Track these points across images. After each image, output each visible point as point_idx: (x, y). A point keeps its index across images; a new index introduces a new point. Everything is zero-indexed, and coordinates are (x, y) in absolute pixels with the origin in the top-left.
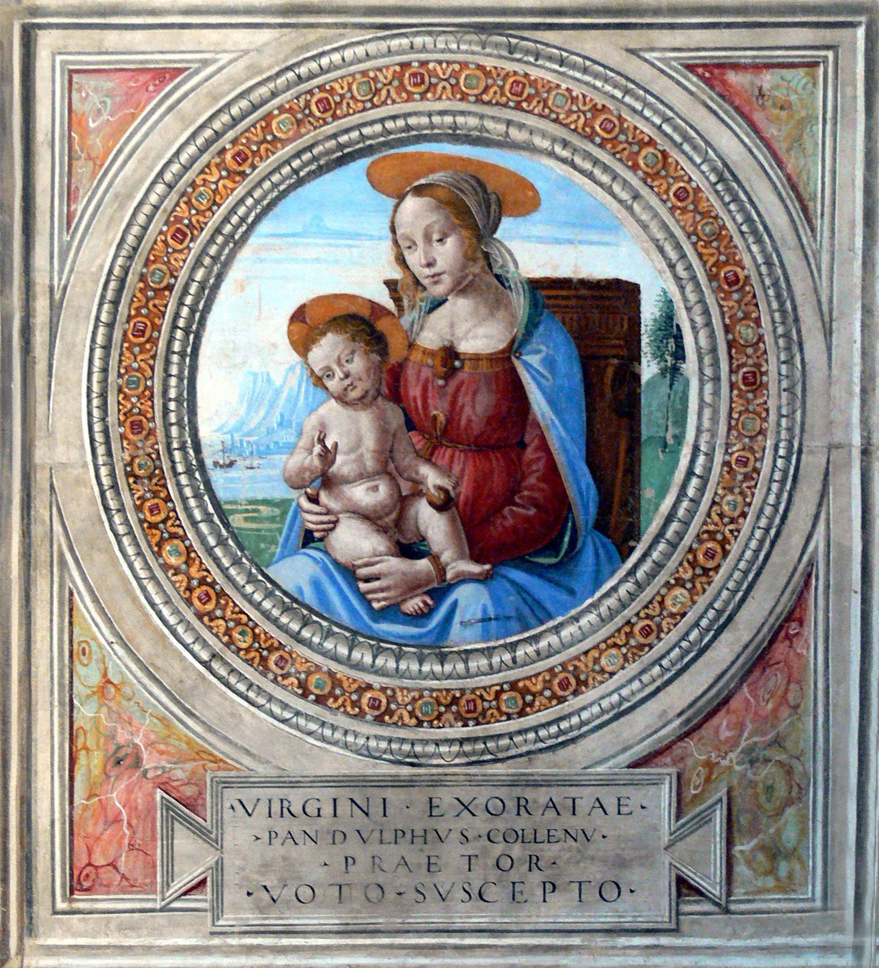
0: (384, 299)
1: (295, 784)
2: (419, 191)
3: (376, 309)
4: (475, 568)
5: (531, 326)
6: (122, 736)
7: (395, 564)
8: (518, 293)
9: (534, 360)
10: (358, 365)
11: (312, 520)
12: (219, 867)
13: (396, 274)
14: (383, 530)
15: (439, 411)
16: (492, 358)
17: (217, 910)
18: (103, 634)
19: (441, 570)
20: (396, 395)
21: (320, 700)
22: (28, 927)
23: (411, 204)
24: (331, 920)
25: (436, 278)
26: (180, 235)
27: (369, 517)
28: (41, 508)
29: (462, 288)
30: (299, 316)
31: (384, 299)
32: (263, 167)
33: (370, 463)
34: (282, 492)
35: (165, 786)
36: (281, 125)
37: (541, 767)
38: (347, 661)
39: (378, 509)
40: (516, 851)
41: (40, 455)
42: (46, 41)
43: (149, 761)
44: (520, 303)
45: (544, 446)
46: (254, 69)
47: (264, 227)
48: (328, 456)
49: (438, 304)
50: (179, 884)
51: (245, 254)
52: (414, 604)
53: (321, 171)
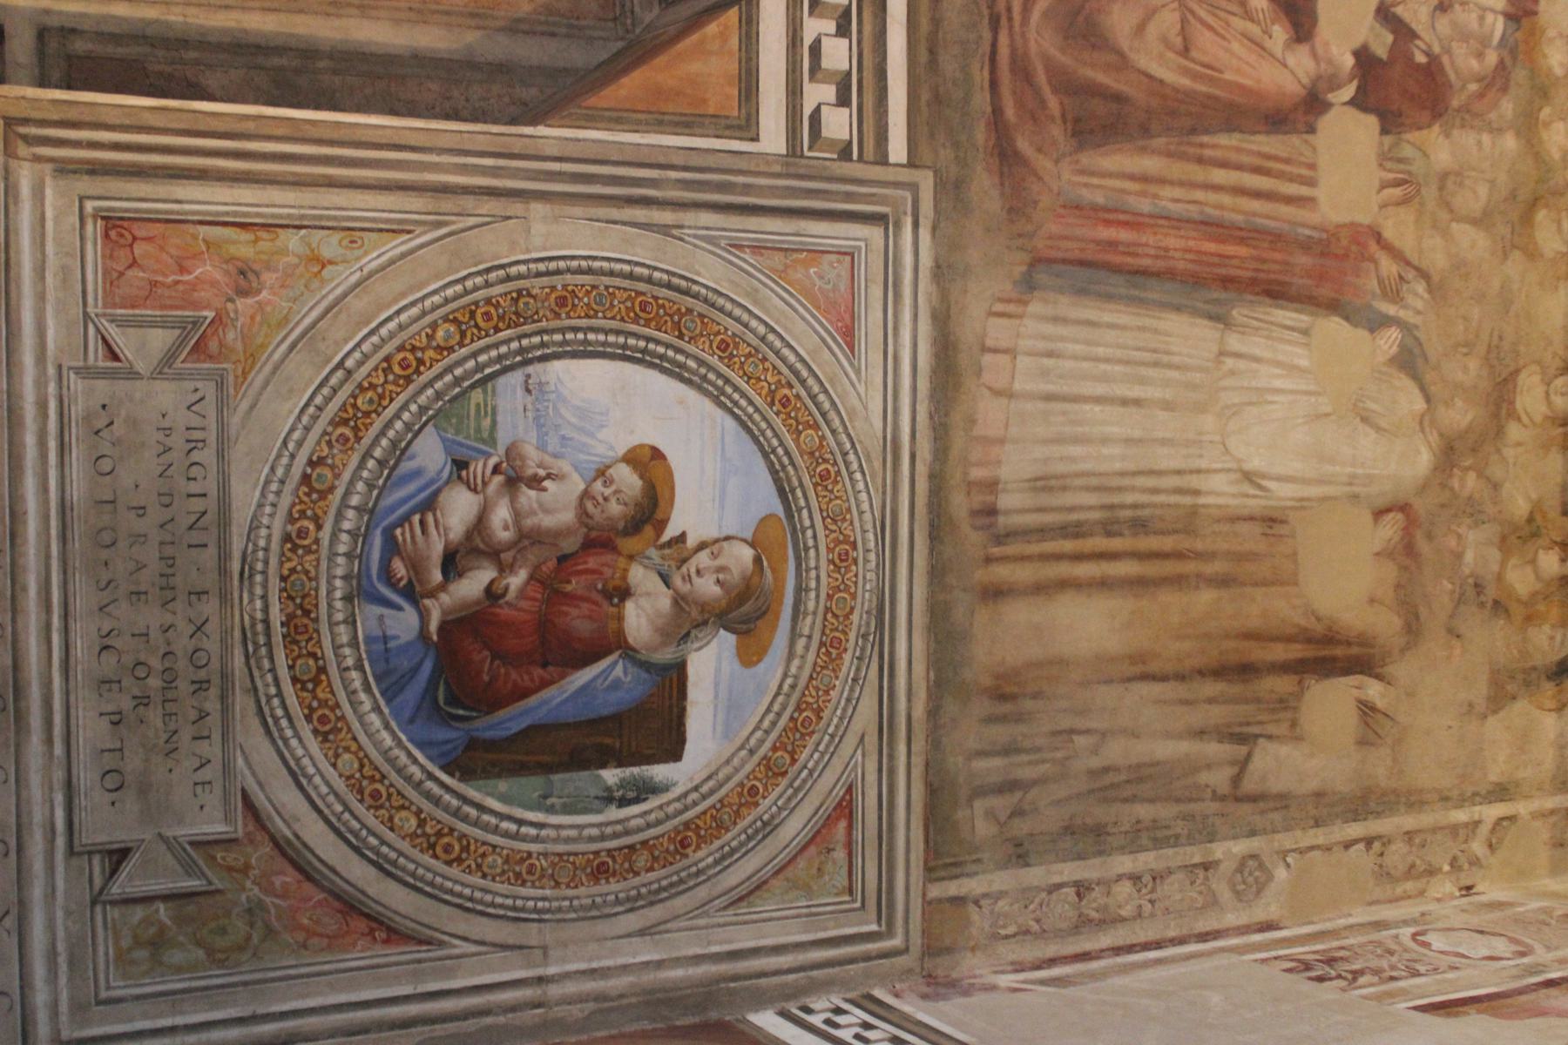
0: (670, 532)
2: (757, 560)
3: (661, 525)
4: (433, 626)
5: (646, 666)
6: (269, 278)
7: (438, 548)
10: (615, 508)
11: (478, 468)
12: (133, 375)
13: (691, 542)
14: (469, 535)
15: (573, 586)
16: (620, 633)
17: (85, 372)
18: (371, 261)
19: (432, 594)
21: (306, 479)
22: (64, 169)
23: (747, 553)
24: (77, 492)
25: (688, 578)
27: (480, 522)
28: (490, 206)
29: (679, 601)
30: (657, 454)
31: (670, 532)
32: (778, 422)
33: (529, 522)
34: (504, 438)
35: (218, 321)
37: (242, 702)
41: (538, 209)
42: (874, 233)
44: (666, 655)
45: (545, 684)
46: (852, 413)
47: (730, 423)
48: (535, 482)
50: (113, 332)
51: (708, 405)
52: (400, 568)
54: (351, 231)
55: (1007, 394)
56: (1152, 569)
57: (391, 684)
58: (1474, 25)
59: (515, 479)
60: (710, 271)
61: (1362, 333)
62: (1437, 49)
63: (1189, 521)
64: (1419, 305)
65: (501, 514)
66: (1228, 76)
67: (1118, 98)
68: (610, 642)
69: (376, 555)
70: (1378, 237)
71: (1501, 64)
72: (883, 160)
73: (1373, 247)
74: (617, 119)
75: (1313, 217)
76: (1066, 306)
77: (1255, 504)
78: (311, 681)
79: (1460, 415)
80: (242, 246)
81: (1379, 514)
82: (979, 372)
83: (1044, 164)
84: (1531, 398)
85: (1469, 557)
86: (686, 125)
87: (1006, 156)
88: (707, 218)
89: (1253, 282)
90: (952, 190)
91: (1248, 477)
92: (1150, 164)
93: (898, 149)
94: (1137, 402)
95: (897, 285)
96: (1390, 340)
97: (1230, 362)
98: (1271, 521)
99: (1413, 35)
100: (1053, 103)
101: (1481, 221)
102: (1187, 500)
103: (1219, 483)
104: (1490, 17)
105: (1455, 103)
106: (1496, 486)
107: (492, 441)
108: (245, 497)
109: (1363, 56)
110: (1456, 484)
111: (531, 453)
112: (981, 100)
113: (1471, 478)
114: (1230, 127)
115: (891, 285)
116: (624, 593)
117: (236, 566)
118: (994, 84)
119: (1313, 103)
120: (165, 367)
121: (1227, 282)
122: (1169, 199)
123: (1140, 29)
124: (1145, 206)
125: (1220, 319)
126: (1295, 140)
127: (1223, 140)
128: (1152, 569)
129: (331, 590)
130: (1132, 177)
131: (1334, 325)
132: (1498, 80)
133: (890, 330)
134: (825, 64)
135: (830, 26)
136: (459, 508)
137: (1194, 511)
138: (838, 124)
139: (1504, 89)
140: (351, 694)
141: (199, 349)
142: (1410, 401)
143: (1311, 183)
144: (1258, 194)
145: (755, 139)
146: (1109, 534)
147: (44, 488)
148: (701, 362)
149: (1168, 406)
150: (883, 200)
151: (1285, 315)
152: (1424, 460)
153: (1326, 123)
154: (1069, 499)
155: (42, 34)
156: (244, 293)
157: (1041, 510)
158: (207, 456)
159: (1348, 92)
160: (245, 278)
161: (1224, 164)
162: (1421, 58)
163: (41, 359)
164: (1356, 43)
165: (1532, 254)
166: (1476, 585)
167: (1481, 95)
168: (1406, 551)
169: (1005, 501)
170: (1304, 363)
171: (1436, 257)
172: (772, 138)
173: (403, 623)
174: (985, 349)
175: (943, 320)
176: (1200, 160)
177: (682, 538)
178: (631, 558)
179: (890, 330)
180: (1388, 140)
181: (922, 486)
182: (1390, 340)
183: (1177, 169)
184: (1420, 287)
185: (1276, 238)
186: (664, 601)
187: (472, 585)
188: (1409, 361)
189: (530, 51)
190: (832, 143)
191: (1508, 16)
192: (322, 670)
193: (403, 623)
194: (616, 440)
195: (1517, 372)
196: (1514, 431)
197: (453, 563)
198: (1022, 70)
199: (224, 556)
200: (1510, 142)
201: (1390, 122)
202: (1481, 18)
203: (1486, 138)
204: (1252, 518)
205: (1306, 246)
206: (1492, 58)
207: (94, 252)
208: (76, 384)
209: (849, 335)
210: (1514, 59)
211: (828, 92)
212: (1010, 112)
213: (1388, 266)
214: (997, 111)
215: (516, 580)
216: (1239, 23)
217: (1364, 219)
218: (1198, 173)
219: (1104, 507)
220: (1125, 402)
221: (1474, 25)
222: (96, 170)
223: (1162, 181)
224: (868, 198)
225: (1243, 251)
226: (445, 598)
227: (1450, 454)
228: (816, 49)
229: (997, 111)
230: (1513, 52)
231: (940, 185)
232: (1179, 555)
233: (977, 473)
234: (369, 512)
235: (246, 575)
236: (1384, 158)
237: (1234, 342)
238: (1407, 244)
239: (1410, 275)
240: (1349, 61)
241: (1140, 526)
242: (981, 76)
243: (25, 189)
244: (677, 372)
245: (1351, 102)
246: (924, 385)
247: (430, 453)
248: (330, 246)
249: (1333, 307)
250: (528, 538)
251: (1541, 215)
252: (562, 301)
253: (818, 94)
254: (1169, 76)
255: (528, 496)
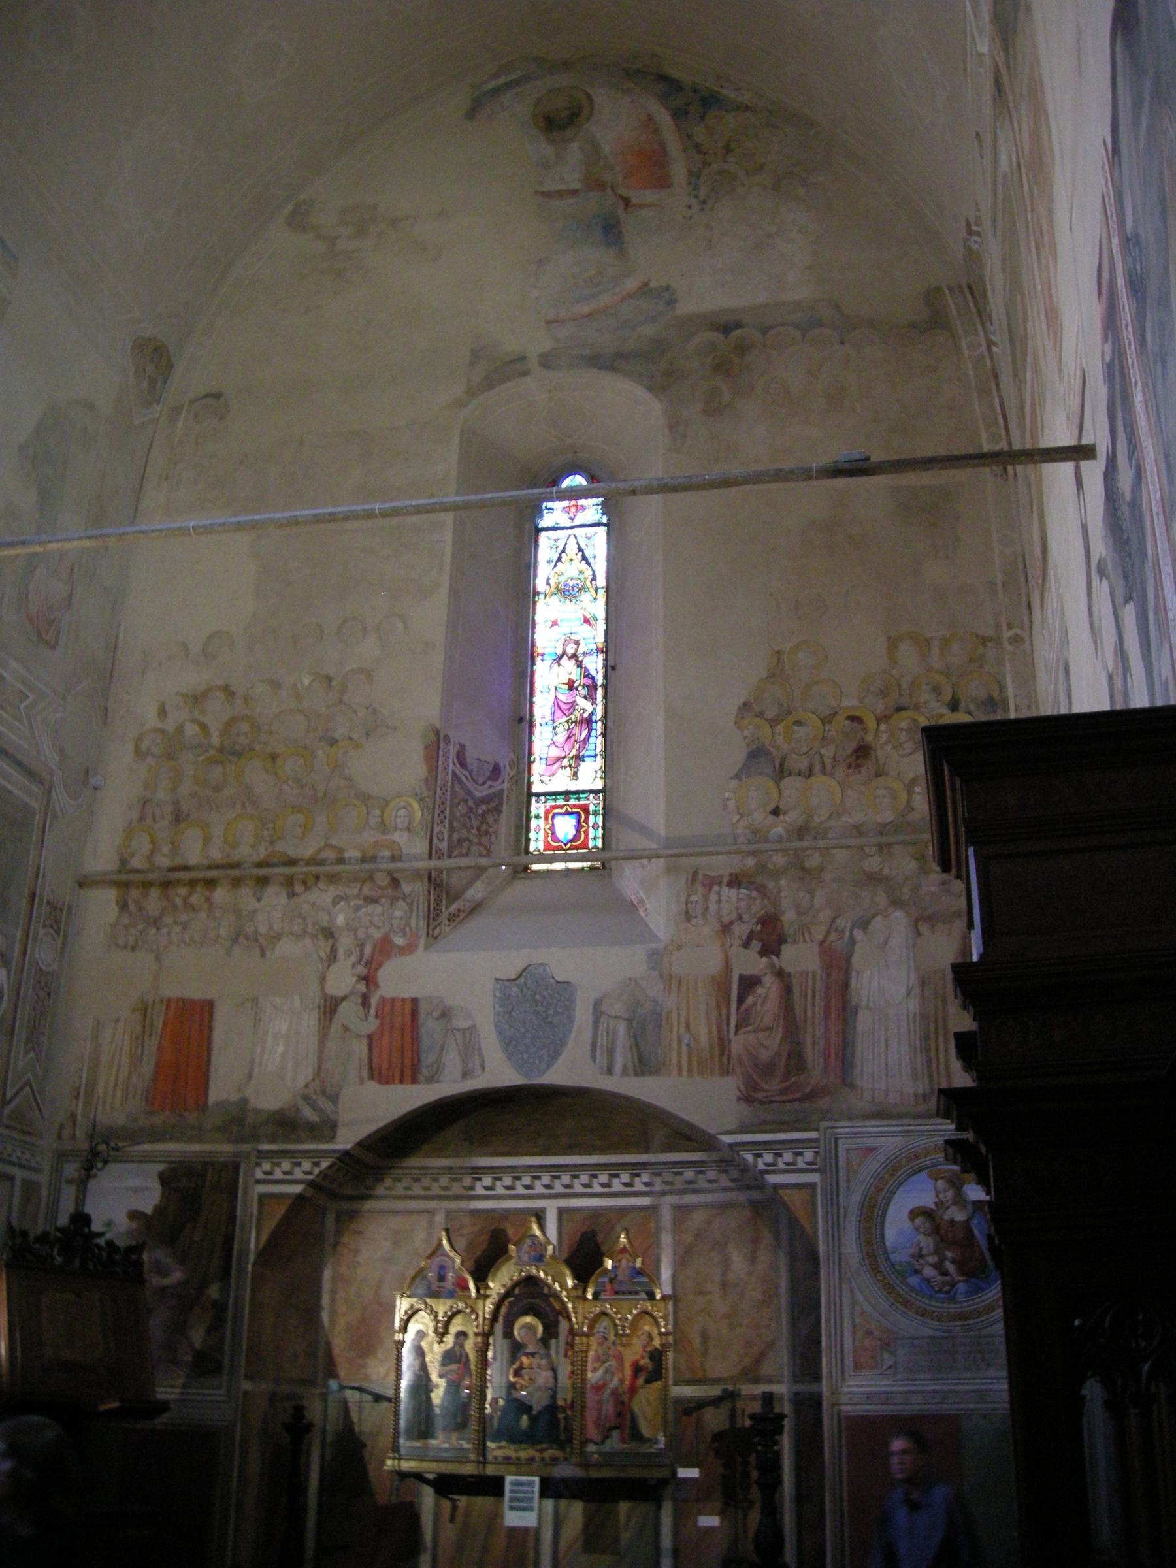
0: (933, 1207)
1: (916, 1338)
2: (942, 1178)
3: (932, 1210)
4: (961, 1278)
5: (974, 1212)
6: (868, 1326)
7: (939, 1278)
8: (955, 1135)
9: (975, 1222)
10: (928, 1225)
11: (917, 1267)
12: (895, 1362)
13: (937, 1200)
14: (936, 1269)
15: (950, 1236)
16: (964, 1222)
17: (895, 1374)
18: (861, 1299)
19: (953, 1279)
20: (938, 1233)
21: (922, 1315)
22: (843, 1379)
23: (940, 1182)
24: (927, 1376)
25: (947, 1201)
26: (878, 1191)
27: (933, 1265)
28: (843, 1264)
29: (955, 1204)
30: (911, 1212)
31: (933, 1207)
32: (900, 1173)
33: (932, 1251)
34: (908, 1259)
35: (880, 1340)
36: (903, 1163)
37: (985, 1332)
38: (930, 1305)
39: (446, 1404)
40: (978, 1356)
41: (843, 1251)
42: (841, 1142)
43: (876, 1333)
44: (970, 1207)
45: (978, 1246)
46: (895, 1148)
47: (901, 1189)
48: (921, 1249)
49: (948, 1208)
50: (884, 1368)
51: (896, 1196)
52: (946, 1288)
53: (916, 1173)
54: (854, 1303)
55: (887, 1090)
56: (941, 1031)
57: (979, 1290)
58: (745, 903)
59: (920, 1256)
60: (856, 1198)
61: (857, 947)
62: (755, 920)
63: (924, 1017)
64: (844, 921)
65: (930, 1259)
66: (776, 1011)
67: (789, 1054)
68: (967, 1223)
69: (942, 1296)
70: (823, 942)
71: (756, 889)
72: (817, 1140)
73: (826, 944)
74: (815, 1228)
75: (819, 971)
76: (857, 1071)
77: (917, 991)
78: (978, 1313)
79: (882, 899)
80: (859, 1334)
81: (919, 934)
82: (880, 1103)
83: (813, 1082)
84: (873, 864)
85: (933, 889)
86: (814, 1205)
87: (812, 1096)
88: (841, 1197)
89: (843, 996)
90: (825, 1115)
91: (908, 993)
92: (809, 1041)
93: (813, 1135)
94: (886, 1040)
95: (856, 1134)
96: (858, 934)
97: (871, 1004)
98: (923, 983)
99: (751, 932)
100: (793, 1079)
101: (811, 893)
102: (918, 1019)
103: (911, 1008)
104: (741, 896)
105: (772, 910)
106: (906, 878)
107: (909, 1263)
108: (927, 1332)
109: (763, 953)
110: (907, 897)
111: (912, 1251)
112: (796, 1105)
113: (905, 890)
114: (793, 1010)
115: (854, 1135)
116: (952, 1222)
117: (945, 1334)
118: (790, 1101)
119: (780, 974)
120: (893, 1353)
121: (844, 1008)
122: (819, 1033)
123: (766, 1047)
124: (822, 1042)
125: (856, 1010)
126: (794, 981)
127: (797, 1012)
128: (941, 1031)
129: (952, 1308)
130: (814, 1049)
131: (855, 960)
132: (761, 889)
133: (869, 1135)
134: (791, 1161)
135: (780, 1159)
136: (929, 1272)
137: (921, 1014)
138: (809, 1155)
139: (764, 886)
140: (982, 1302)
141: (888, 1344)
142: (878, 923)
143: (807, 973)
144: (814, 996)
145: (816, 1183)
146: (930, 1049)
147: (927, 1385)
148: (883, 1199)
149: (887, 1029)
150: (830, 1139)
151: (853, 983)
152: (899, 915)
153: (788, 968)
154: (919, 1067)
155: (796, 1382)
156: (872, 1333)
157: (923, 1078)
158: (916, 1342)
159: (774, 958)
160: (869, 1333)
161: (805, 1012)
162: (759, 927)
163: (894, 1386)
164: (757, 956)
165: (821, 868)
166: (943, 884)
167: (769, 898)
168: (931, 919)
169: (920, 1090)
170: (869, 972)
171: (825, 915)
172: (815, 1178)
173: (961, 1287)
174: (873, 1101)
175: (866, 1117)
176: (805, 1021)
177: (936, 1203)
178: (942, 1219)
179: (869, 1135)
180: (789, 940)
181: (919, 1121)
182: (858, 934)
183: (809, 1030)
184: (838, 921)
185: (828, 988)
186: (953, 1208)
187: (950, 1267)
188: (864, 924)
189: (784, 1235)
190: (815, 1158)
191: (739, 888)
192: (975, 1310)
193: (961, 1287)
194: (907, 1225)
195: (864, 871)
196: (886, 871)
197: (945, 1273)
198: (784, 1091)
199: (943, 1338)
200: (783, 882)
201: (782, 940)
202: (742, 900)
203: (783, 894)
204: (922, 991)
205: (829, 975)
206: (755, 894)
207: (863, 1372)
208: (899, 1377)
209: (871, 1150)
210: (753, 883)
211: (800, 1159)
212: (798, 1095)
213: (832, 937)
214: (799, 1099)
215: (949, 1254)
216: (759, 1007)
217: (816, 949)
218: (809, 1021)
219: (921, 1053)
220: (887, 1046)
221: (745, 903)
222: (843, 1372)
223: (814, 1037)
224: (830, 1144)
225: (833, 1001)
226: (955, 1275)
227: (896, 902)
228: (787, 1164)
229: (799, 1099)
230: (751, 883)
231: (823, 1119)
232: (936, 1021)
233: (912, 1102)
234: (931, 1297)
235: (949, 1331)
236: (795, 942)
237: (864, 1003)
238: (824, 928)
239: (834, 926)
240: (764, 960)
241: (926, 1038)
242: (788, 1106)
243: (849, 1389)
244: (887, 1205)
245: (778, 956)
246: (885, 1123)
247: (914, 1280)
248: (858, 1309)
249: (848, 960)
250: (937, 1251)
251: (807, 865)
252: (869, 1242)
253: (801, 1163)
254: (780, 1035)
255: (925, 1251)
